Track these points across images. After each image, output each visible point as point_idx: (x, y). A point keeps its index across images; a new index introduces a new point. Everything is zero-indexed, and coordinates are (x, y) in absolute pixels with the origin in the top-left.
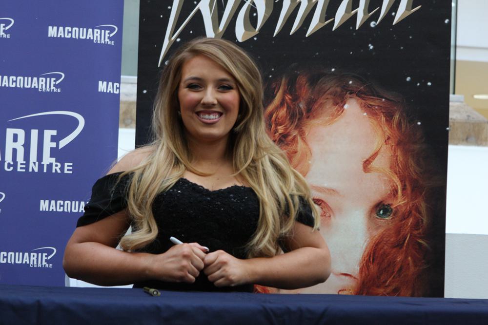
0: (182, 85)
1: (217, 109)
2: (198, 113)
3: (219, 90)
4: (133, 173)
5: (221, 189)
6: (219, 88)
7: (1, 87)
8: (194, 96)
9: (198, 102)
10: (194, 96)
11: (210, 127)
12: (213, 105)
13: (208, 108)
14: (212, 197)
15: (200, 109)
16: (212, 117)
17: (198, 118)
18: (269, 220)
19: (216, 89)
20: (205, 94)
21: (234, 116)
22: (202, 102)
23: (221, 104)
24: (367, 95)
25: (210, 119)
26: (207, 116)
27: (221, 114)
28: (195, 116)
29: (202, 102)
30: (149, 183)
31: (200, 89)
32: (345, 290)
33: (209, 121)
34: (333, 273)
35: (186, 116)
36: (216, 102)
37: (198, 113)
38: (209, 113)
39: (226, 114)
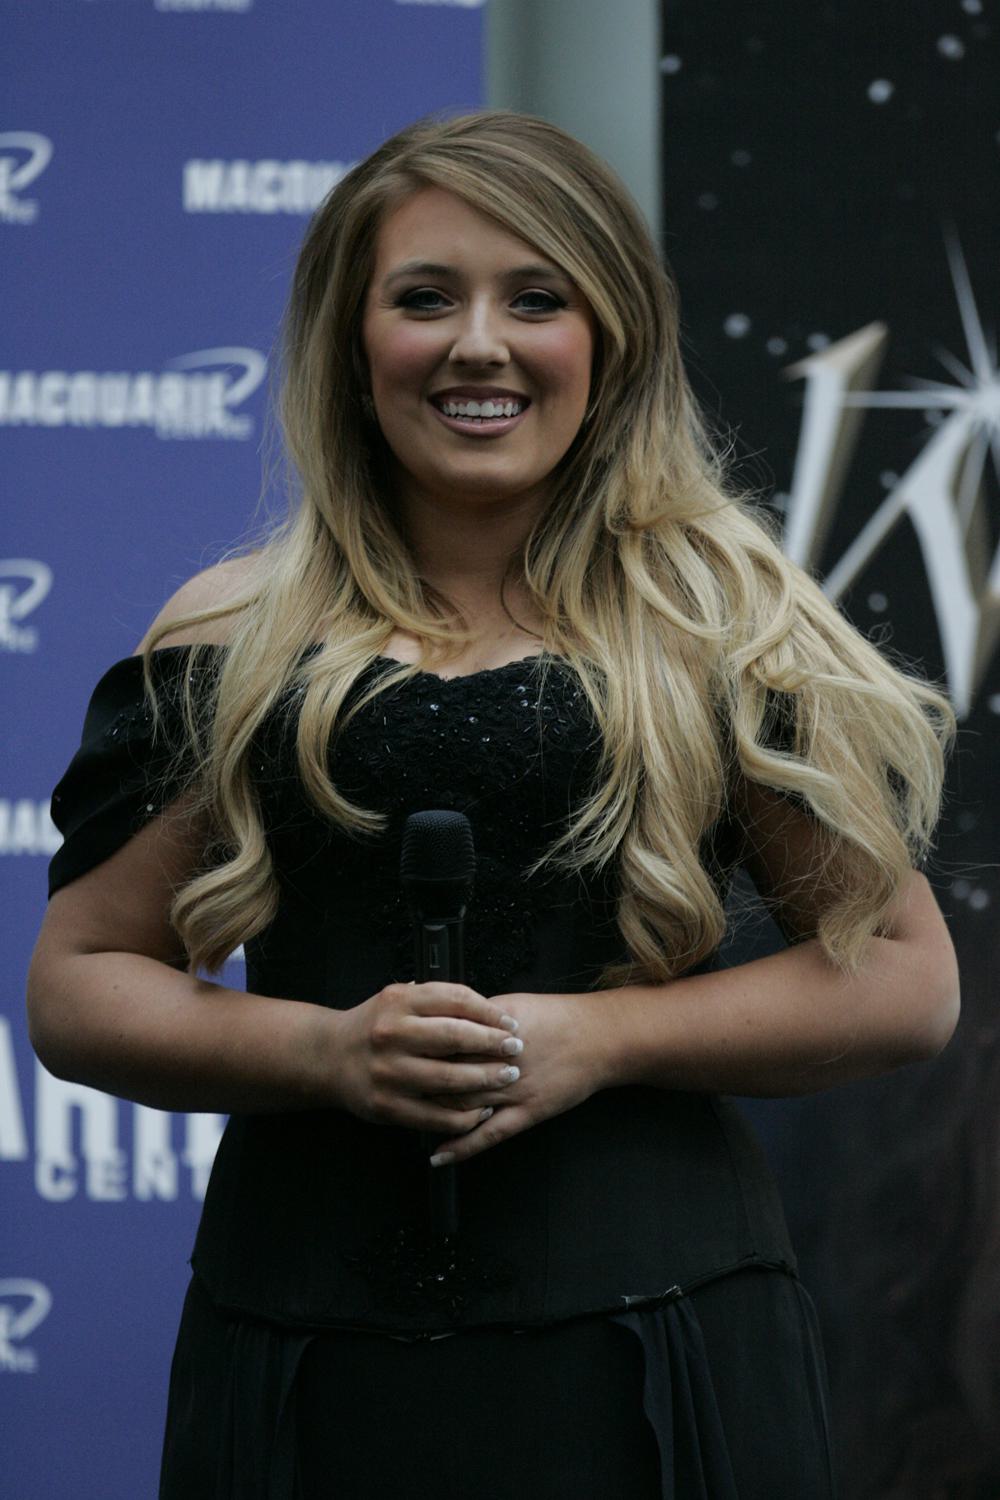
0: (377, 292)
1: (509, 381)
2: (438, 401)
3: (515, 311)
4: (190, 648)
5: (487, 672)
6: (513, 305)
7: (17, 1173)
8: (424, 336)
9: (440, 359)
10: (424, 336)
11: (481, 449)
12: (496, 365)
13: (476, 374)
14: (446, 698)
15: (447, 382)
16: (490, 408)
17: (439, 419)
18: (658, 882)
19: (505, 305)
20: (466, 326)
21: (570, 411)
22: (453, 355)
23: (521, 362)
24: (340, 205)
25: (482, 418)
26: (472, 408)
27: (524, 402)
28: (427, 410)
29: (453, 355)
30: (221, 607)
31: (448, 309)
32: (313, 650)
33: (478, 427)
34: (639, 898)
35: (394, 413)
36: (503, 354)
37: (438, 401)
38: (481, 397)
39: (541, 403)
